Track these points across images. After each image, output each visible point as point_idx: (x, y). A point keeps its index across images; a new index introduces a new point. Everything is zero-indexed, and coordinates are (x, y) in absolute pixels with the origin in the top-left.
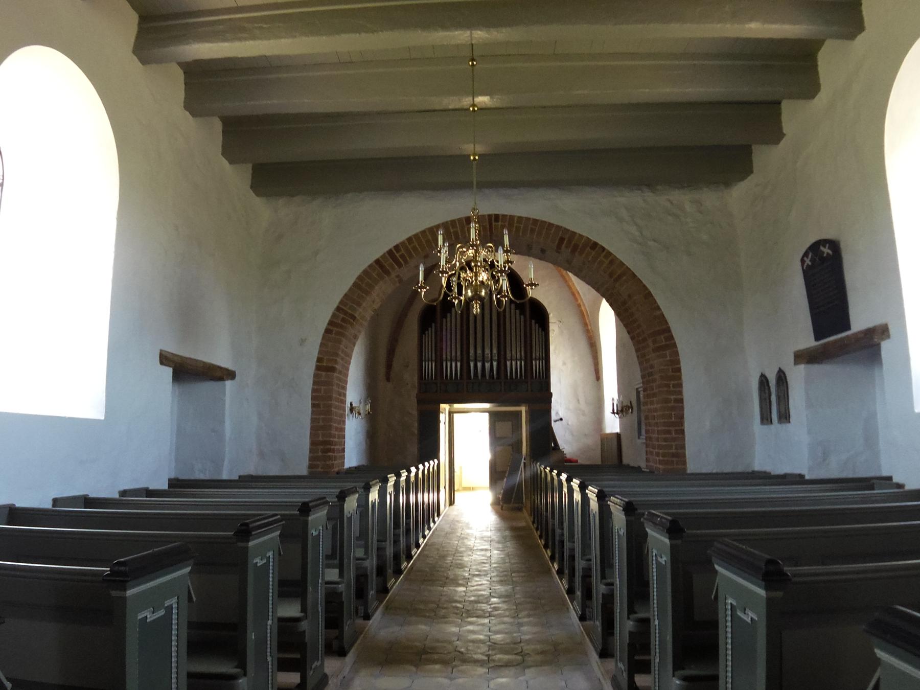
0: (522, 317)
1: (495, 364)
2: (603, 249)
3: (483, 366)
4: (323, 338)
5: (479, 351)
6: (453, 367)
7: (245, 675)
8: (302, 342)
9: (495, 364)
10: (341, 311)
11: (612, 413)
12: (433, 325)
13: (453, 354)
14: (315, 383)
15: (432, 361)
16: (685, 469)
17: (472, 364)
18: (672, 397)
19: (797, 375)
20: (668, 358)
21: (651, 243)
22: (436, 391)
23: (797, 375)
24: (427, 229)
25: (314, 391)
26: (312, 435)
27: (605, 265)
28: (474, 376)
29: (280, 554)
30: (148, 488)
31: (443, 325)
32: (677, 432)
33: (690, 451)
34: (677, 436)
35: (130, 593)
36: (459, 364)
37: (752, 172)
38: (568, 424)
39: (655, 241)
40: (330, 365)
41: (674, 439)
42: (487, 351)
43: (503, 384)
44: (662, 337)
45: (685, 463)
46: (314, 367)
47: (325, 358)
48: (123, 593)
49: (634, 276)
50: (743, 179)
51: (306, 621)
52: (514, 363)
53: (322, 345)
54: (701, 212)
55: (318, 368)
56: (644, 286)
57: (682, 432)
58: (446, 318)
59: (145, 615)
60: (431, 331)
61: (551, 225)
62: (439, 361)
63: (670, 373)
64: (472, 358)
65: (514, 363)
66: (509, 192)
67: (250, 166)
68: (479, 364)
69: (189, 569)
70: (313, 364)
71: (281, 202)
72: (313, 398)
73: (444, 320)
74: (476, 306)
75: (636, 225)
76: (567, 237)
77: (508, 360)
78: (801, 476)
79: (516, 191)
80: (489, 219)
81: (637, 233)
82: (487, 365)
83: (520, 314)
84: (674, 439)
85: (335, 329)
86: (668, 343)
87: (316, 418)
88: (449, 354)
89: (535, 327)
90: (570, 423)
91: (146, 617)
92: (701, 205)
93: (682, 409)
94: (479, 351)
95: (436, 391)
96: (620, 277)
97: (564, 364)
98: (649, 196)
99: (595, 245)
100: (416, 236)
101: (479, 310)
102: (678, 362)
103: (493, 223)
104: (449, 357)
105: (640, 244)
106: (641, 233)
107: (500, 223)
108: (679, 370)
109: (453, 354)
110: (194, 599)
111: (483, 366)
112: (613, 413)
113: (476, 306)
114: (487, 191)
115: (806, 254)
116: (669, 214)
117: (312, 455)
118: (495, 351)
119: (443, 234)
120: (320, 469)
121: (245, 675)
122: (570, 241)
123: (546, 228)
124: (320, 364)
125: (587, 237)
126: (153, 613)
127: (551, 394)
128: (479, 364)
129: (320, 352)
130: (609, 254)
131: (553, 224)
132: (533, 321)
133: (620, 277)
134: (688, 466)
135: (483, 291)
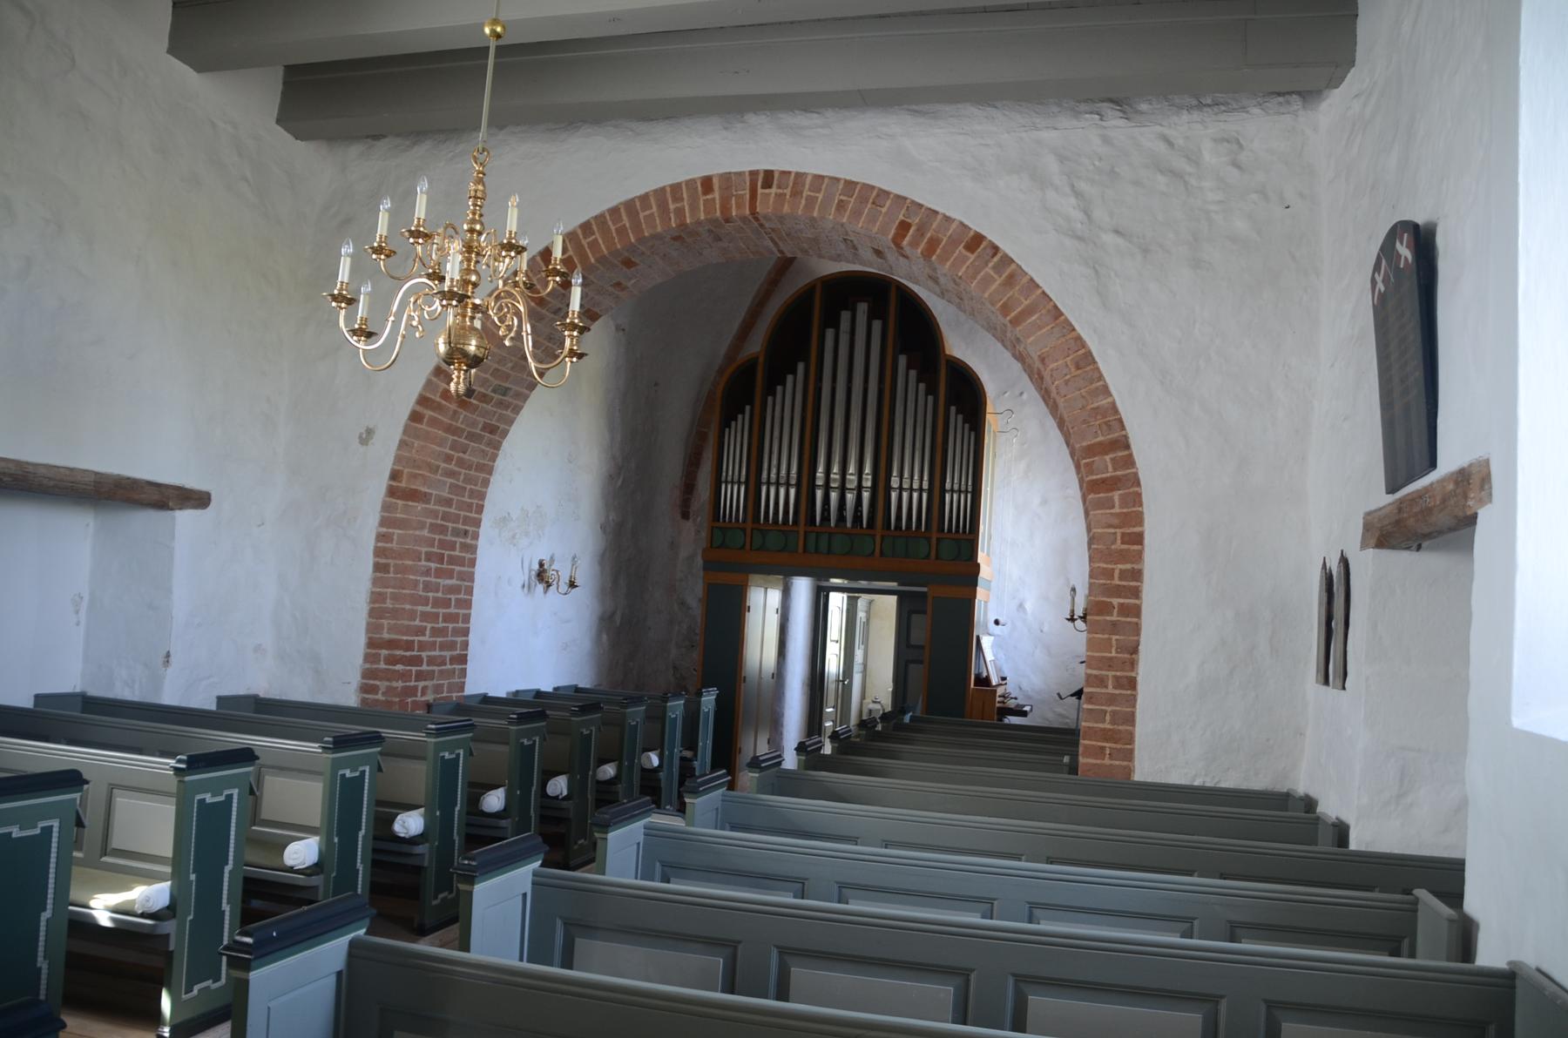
0: (930, 398)
1: (866, 495)
2: (995, 249)
3: (842, 499)
4: (405, 432)
6: (780, 498)
8: (367, 437)
9: (866, 495)
10: (442, 376)
11: (1068, 620)
12: (748, 408)
13: (783, 472)
14: (384, 522)
15: (788, 485)
16: (1129, 771)
18: (1116, 601)
19: (1368, 566)
20: (1117, 510)
21: (1109, 239)
22: (743, 547)
23: (1368, 566)
24: (621, 204)
25: (381, 537)
26: (372, 628)
27: (994, 287)
28: (793, 522)
30: (258, 695)
32: (1118, 683)
33: (1144, 729)
34: (1117, 692)
36: (792, 491)
37: (1352, 63)
38: (1042, 631)
39: (1117, 232)
40: (413, 487)
41: (1112, 700)
43: (878, 539)
44: (1108, 458)
45: (1129, 755)
46: (383, 490)
47: (406, 471)
49: (1057, 313)
50: (1335, 82)
53: (403, 444)
54: (1236, 164)
55: (392, 492)
56: (1079, 338)
57: (1132, 683)
58: (774, 395)
60: (742, 422)
61: (884, 194)
62: (754, 485)
63: (1118, 545)
64: (820, 482)
66: (800, 119)
67: (279, 73)
68: (834, 496)
70: (381, 483)
71: (355, 150)
72: (378, 552)
73: (770, 399)
74: (459, 377)
75: (1078, 194)
76: (915, 221)
77: (948, 491)
79: (814, 119)
80: (751, 180)
81: (1077, 215)
83: (927, 393)
84: (1112, 700)
85: (428, 413)
86: (1119, 473)
87: (380, 594)
88: (774, 471)
89: (957, 420)
90: (1046, 629)
92: (1241, 146)
93: (1137, 629)
95: (743, 547)
96: (1028, 312)
97: (1044, 502)
98: (1116, 124)
99: (978, 239)
100: (600, 219)
101: (462, 385)
102: (1138, 519)
103: (760, 191)
104: (729, 479)
105: (1080, 239)
106: (1087, 213)
107: (774, 190)
108: (1138, 539)
109: (783, 472)
111: (842, 499)
112: (1072, 619)
113: (459, 377)
114: (752, 118)
115: (1377, 267)
116: (1162, 172)
117: (368, 666)
119: (518, 206)
120: (380, 697)
122: (921, 231)
123: (871, 201)
124: (394, 484)
125: (962, 223)
127: (979, 565)
128: (834, 496)
129: (398, 459)
130: (1007, 260)
131: (887, 193)
132: (953, 409)
133: (1028, 312)
134: (1137, 763)
135: (474, 342)
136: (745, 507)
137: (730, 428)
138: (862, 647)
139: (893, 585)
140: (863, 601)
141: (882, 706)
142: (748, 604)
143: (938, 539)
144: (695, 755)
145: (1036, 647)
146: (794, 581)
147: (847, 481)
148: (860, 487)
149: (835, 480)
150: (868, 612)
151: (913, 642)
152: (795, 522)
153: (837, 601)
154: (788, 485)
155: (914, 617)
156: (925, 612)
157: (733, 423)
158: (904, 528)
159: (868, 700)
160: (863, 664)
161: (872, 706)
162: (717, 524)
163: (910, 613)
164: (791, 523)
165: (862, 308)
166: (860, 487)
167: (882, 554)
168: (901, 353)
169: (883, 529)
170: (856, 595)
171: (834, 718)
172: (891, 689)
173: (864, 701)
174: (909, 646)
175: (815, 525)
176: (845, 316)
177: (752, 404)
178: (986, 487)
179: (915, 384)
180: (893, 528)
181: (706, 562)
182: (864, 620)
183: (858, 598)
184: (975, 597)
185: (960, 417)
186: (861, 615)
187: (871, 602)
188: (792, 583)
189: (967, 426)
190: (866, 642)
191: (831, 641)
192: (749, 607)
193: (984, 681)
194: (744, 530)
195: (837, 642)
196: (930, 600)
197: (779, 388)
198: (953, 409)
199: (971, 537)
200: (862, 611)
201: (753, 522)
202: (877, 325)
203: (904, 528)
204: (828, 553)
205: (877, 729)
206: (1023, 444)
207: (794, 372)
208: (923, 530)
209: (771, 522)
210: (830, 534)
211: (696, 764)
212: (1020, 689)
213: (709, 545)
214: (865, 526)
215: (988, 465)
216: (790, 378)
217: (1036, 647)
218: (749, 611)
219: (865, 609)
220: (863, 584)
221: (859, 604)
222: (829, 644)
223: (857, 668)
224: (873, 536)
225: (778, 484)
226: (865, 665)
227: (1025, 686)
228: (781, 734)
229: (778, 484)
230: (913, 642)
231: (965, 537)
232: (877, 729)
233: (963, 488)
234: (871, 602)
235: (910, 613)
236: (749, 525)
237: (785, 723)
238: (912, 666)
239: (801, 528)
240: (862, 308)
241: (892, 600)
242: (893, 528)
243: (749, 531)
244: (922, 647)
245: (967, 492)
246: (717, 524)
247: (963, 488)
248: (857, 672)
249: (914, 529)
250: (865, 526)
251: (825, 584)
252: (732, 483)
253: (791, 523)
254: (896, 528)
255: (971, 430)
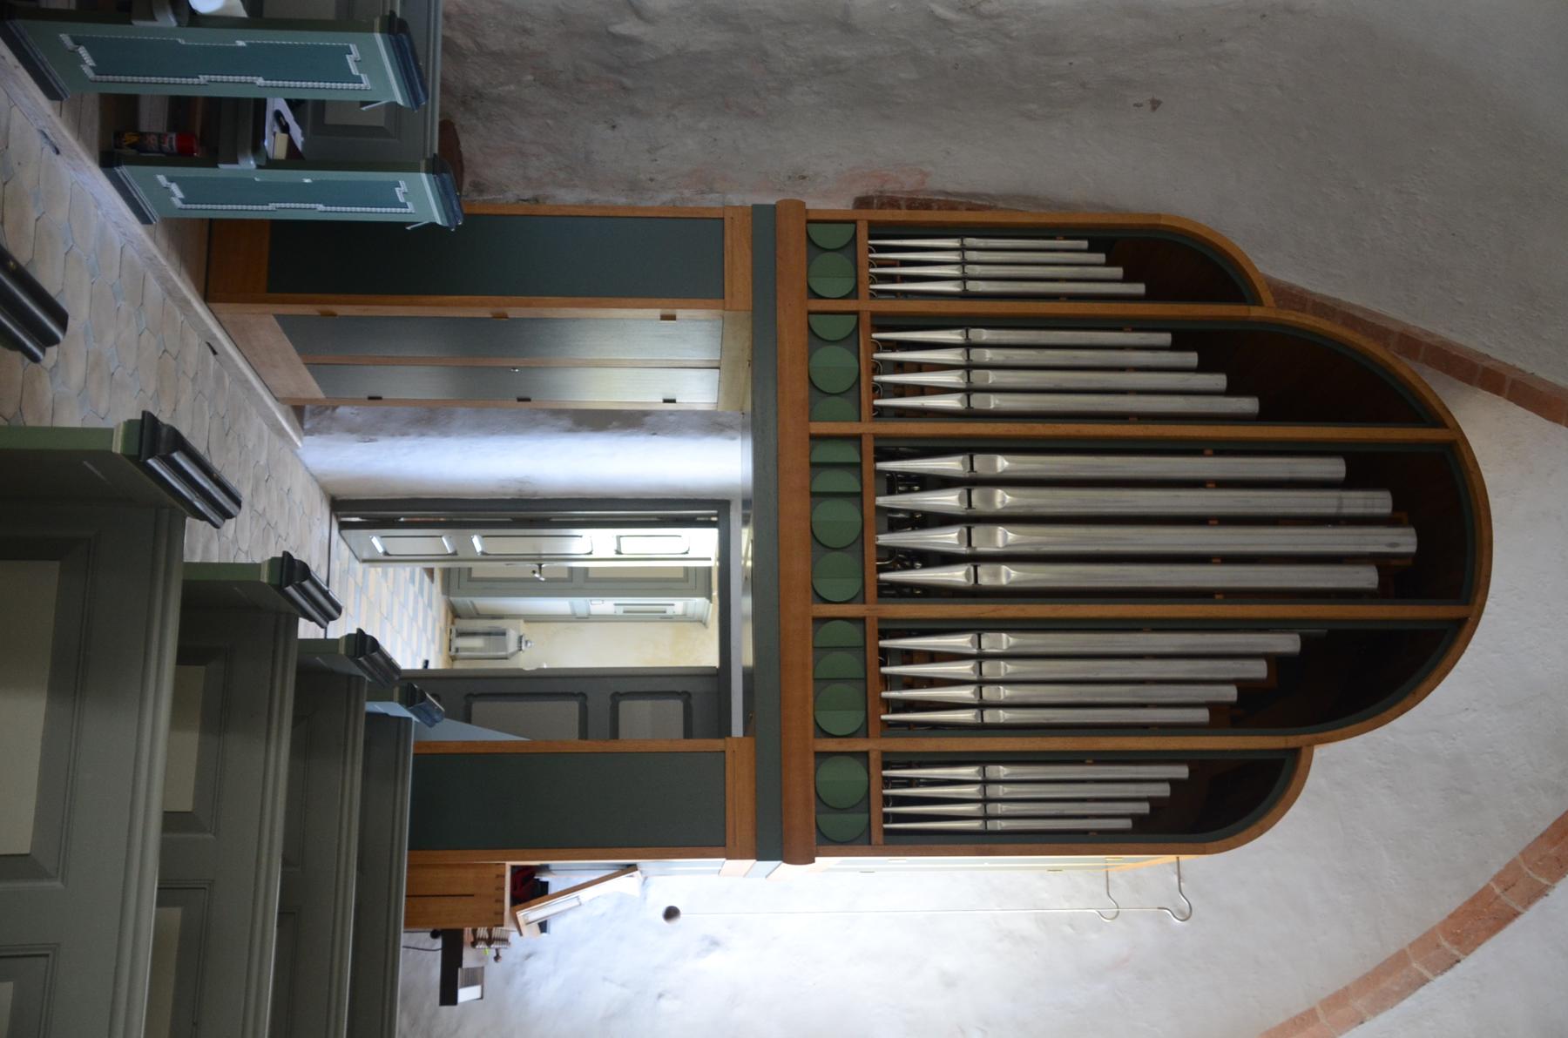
0: (1202, 715)
1: (956, 575)
5: (1003, 499)
7: (259, 167)
9: (956, 575)
13: (993, 378)
15: (964, 279)
17: (951, 465)
22: (814, 295)
28: (882, 408)
29: (364, 104)
31: (1135, 330)
35: (378, 37)
36: (951, 402)
38: (660, 996)
42: (1004, 538)
48: (378, 30)
51: (254, 166)
52: (964, 669)
58: (1175, 347)
59: (364, 81)
60: (1105, 278)
64: (982, 464)
65: (964, 669)
68: (949, 500)
69: (401, 102)
73: (1165, 338)
78: (526, 621)
82: (948, 539)
83: (1214, 707)
89: (1157, 781)
90: (665, 1004)
91: (362, 83)
94: (1003, 499)
95: (814, 295)
97: (949, 982)
109: (993, 378)
110: (364, 109)
118: (1008, 575)
121: (259, 167)
126: (355, 61)
127: (808, 859)
128: (949, 500)
132: (1182, 772)
136: (906, 294)
137: (1090, 250)
138: (620, 611)
139: (745, 654)
140: (705, 607)
141: (513, 654)
142: (680, 313)
143: (865, 755)
144: (272, 164)
145: (623, 985)
146: (738, 442)
147: (990, 528)
148: (975, 559)
149: (990, 500)
150: (684, 618)
151: (625, 705)
152: (880, 413)
153: (700, 545)
154: (968, 391)
155: (676, 706)
156: (688, 733)
157: (1101, 257)
158: (885, 670)
159: (523, 628)
160: (590, 615)
161: (512, 637)
162: (863, 232)
163: (685, 696)
164: (878, 402)
165: (1404, 541)
166: (975, 559)
167: (820, 621)
168: (1305, 641)
169: (881, 620)
170: (715, 593)
171: (460, 556)
172: (545, 666)
173: (522, 621)
174: (617, 697)
175: (877, 460)
176: (1379, 502)
177: (1148, 297)
178: (990, 862)
179: (1233, 676)
180: (884, 643)
181: (773, 209)
182: (670, 611)
183: (709, 597)
184: (730, 856)
185: (1164, 791)
186: (678, 605)
187: (702, 622)
188: (733, 438)
189: (1144, 808)
190: (630, 617)
191: (619, 537)
192: (673, 318)
193: (530, 889)
194: (853, 294)
195: (618, 552)
196: (718, 744)
197: (1192, 358)
198: (1182, 772)
199: (877, 836)
200: (686, 605)
201: (874, 315)
202: (1366, 577)
203: (885, 670)
204: (813, 495)
205: (302, 622)
206: (1071, 926)
207: (1232, 391)
208: (884, 717)
209: (877, 356)
210: (859, 495)
211: (249, 164)
212: (529, 956)
213: (812, 217)
214: (885, 576)
215: (1044, 861)
216: (1219, 381)
217: (623, 985)
218: (664, 318)
219: (690, 611)
220: (743, 604)
221: (698, 600)
222: (609, 534)
223: (581, 604)
224: (860, 598)
225: (968, 367)
226: (588, 618)
227: (535, 967)
228: (404, 434)
229: (968, 367)
230: (625, 705)
231: (876, 818)
232: (302, 622)
233: (993, 809)
234: (702, 622)
235: (685, 696)
236: (865, 305)
237: (427, 440)
238: (573, 706)
239: (868, 427)
240: (1404, 541)
241: (707, 656)
242: (884, 643)
243: (850, 305)
244: (615, 734)
245: (986, 818)
246: (864, 242)
247: (993, 809)
248: (572, 605)
249: (885, 694)
250: (885, 576)
251: (736, 515)
252: (963, 263)
253: (878, 402)
254: (884, 652)
255: (1135, 818)
